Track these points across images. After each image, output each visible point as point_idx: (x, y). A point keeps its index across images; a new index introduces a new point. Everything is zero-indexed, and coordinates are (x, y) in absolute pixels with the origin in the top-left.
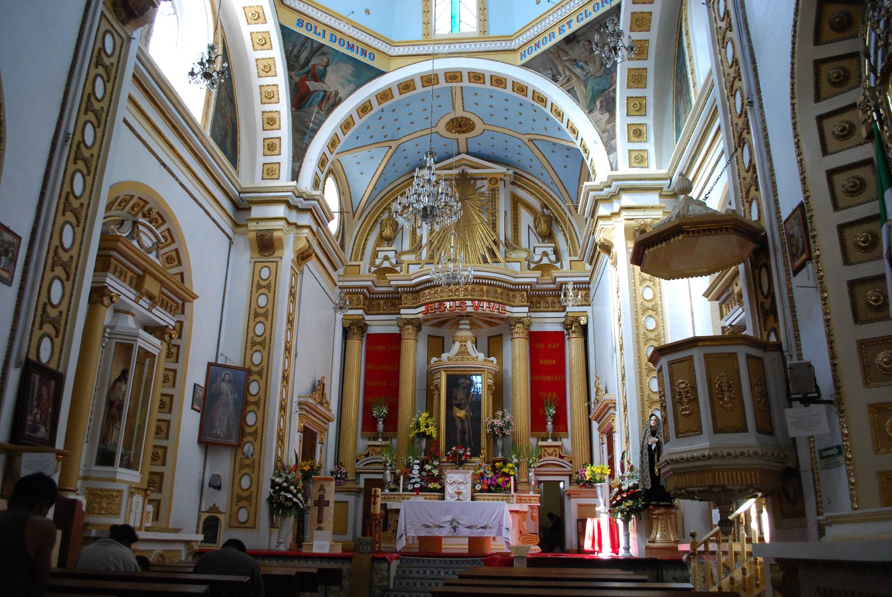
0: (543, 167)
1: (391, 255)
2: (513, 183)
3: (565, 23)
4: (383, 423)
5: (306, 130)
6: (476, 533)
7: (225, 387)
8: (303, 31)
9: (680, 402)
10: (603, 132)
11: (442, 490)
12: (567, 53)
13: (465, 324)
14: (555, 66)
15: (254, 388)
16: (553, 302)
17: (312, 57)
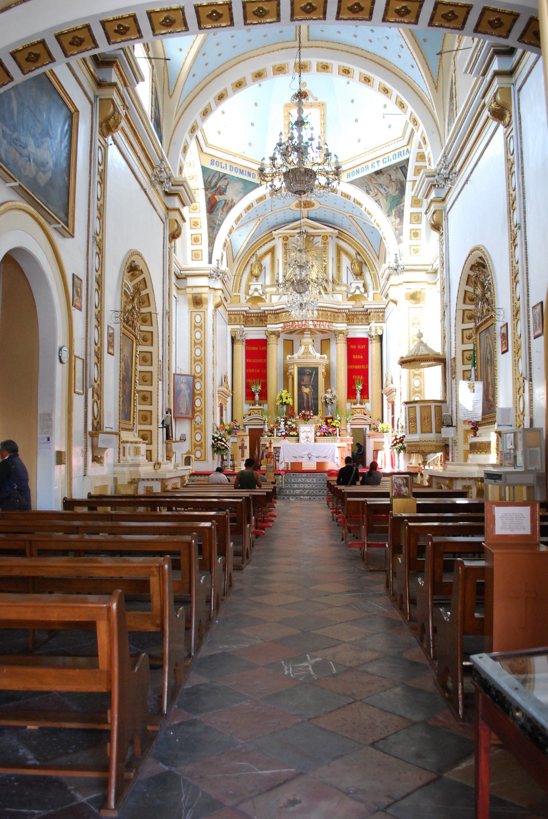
0: (358, 231)
1: (259, 287)
2: (337, 237)
3: (375, 161)
4: (259, 395)
5: (214, 225)
6: (321, 460)
7: (183, 386)
8: (214, 168)
9: (411, 422)
10: (396, 230)
11: (298, 436)
12: (376, 179)
13: (307, 335)
14: (369, 185)
15: (198, 386)
16: (362, 319)
17: (219, 181)
